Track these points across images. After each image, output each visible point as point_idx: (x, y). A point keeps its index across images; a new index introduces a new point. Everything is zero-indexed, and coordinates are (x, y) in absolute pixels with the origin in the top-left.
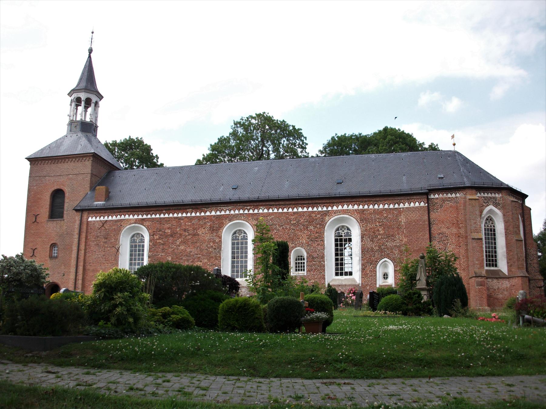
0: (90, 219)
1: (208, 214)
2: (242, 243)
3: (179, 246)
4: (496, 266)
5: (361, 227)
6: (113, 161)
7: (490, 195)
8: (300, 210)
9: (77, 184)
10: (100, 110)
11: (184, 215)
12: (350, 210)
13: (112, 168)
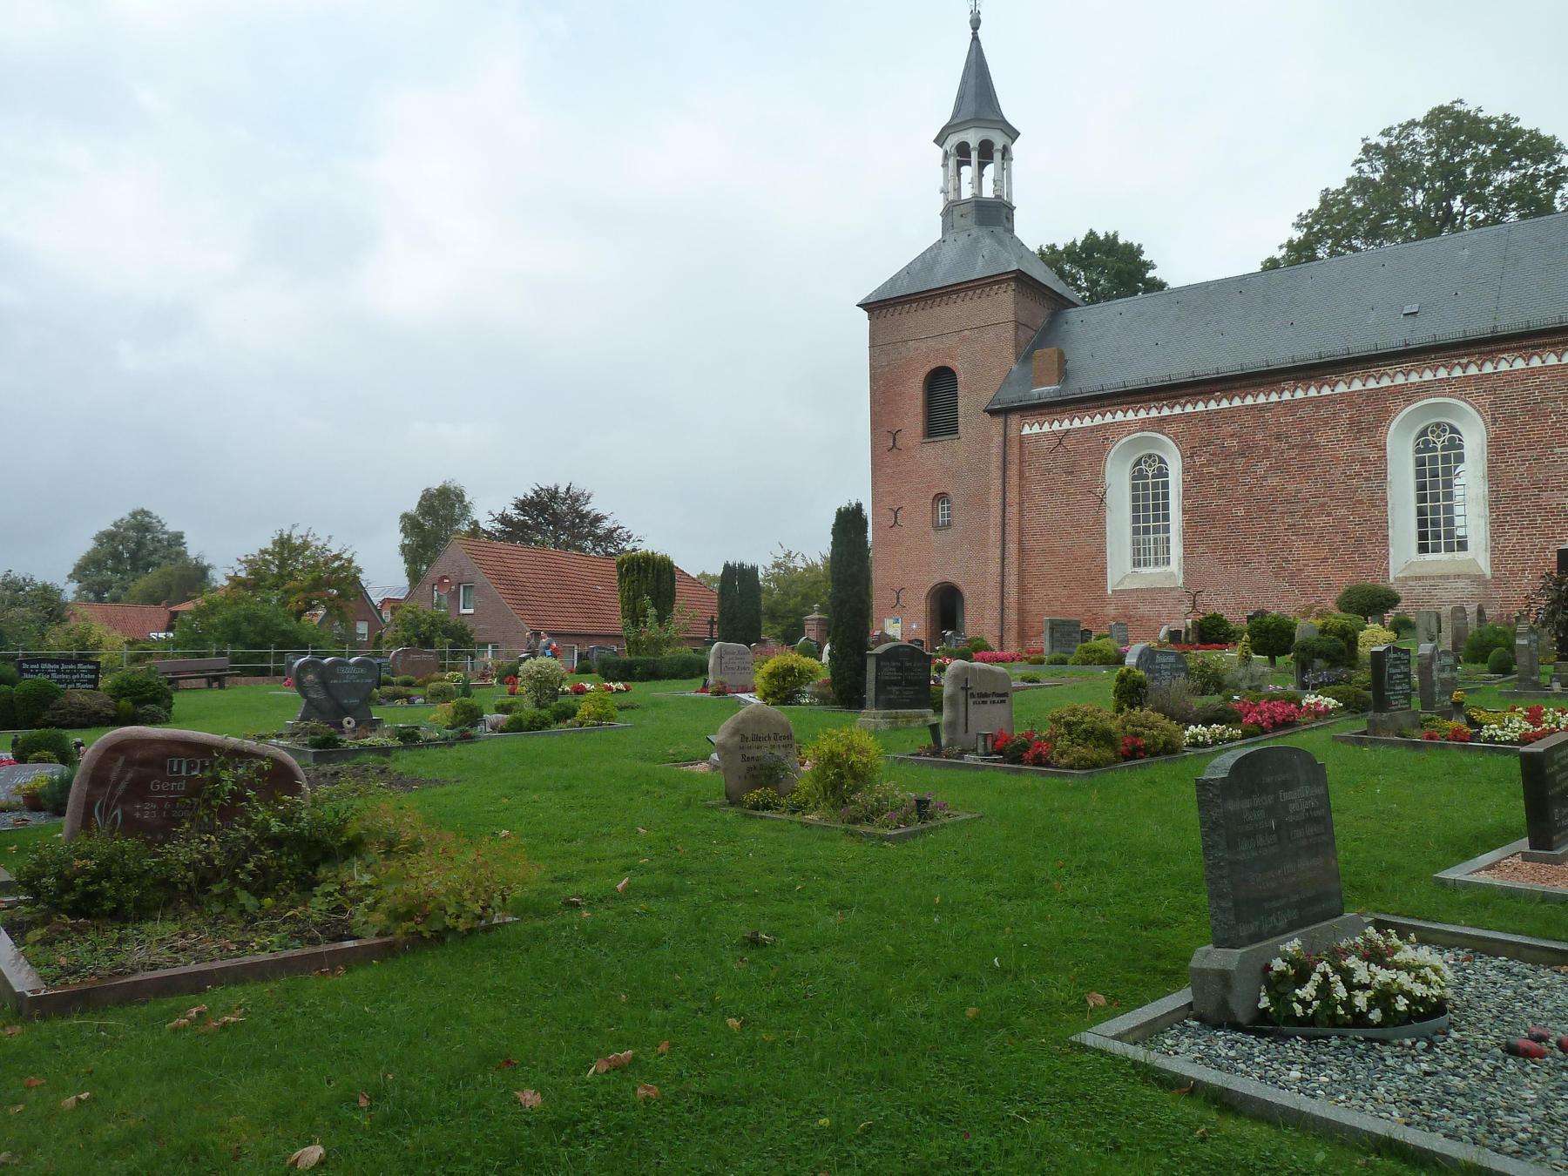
0: (1026, 430)
1: (1341, 388)
2: (1446, 459)
3: (1264, 478)
6: (1059, 286)
9: (983, 349)
11: (1274, 397)
13: (1060, 304)
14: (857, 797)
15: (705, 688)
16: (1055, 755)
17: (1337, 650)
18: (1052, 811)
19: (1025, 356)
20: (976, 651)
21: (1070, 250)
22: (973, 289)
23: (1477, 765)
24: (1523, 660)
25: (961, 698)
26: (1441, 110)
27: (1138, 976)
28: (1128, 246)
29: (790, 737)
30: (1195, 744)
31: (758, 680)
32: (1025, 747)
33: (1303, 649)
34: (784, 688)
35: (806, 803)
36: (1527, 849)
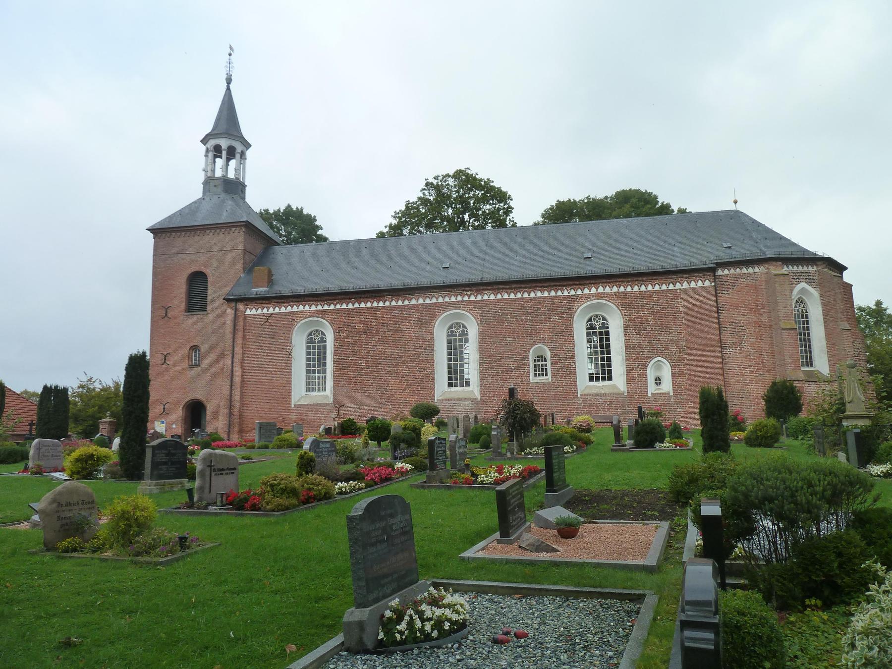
1: (414, 302)
2: (461, 340)
3: (376, 346)
4: (812, 365)
5: (624, 315)
6: (270, 233)
7: (800, 269)
8: (539, 294)
9: (224, 263)
10: (248, 162)
11: (381, 304)
12: (608, 294)
13: (270, 243)
14: (140, 538)
15: (26, 470)
16: (264, 503)
17: (412, 438)
18: (262, 537)
19: (249, 270)
20: (214, 441)
21: (277, 213)
22: (220, 228)
23: (476, 496)
24: (494, 442)
25: (208, 473)
26: (460, 171)
27: (313, 631)
28: (309, 216)
29: (93, 502)
30: (341, 493)
31: (67, 462)
32: (246, 500)
33: (395, 438)
34: (86, 468)
35: (104, 545)
36: (499, 538)
